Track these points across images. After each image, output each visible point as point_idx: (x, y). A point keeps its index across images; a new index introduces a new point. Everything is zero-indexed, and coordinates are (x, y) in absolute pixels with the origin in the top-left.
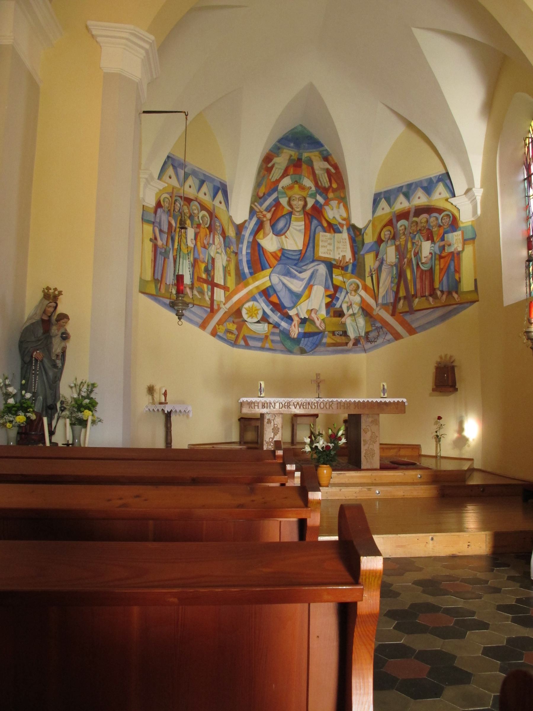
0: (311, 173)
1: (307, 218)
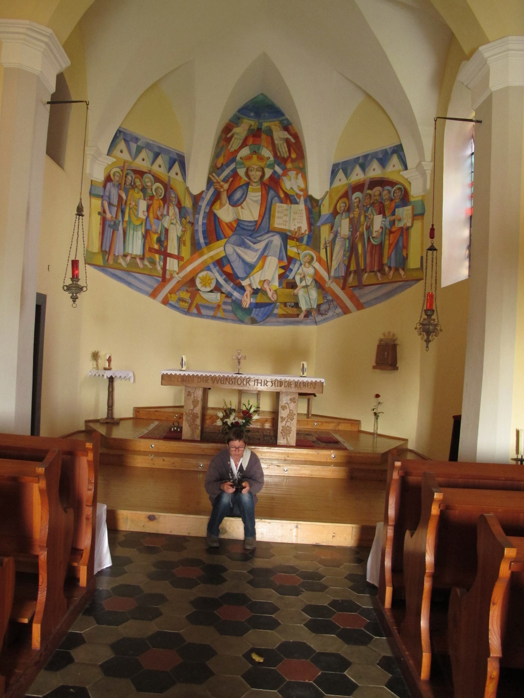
0: (271, 143)
1: (264, 188)
